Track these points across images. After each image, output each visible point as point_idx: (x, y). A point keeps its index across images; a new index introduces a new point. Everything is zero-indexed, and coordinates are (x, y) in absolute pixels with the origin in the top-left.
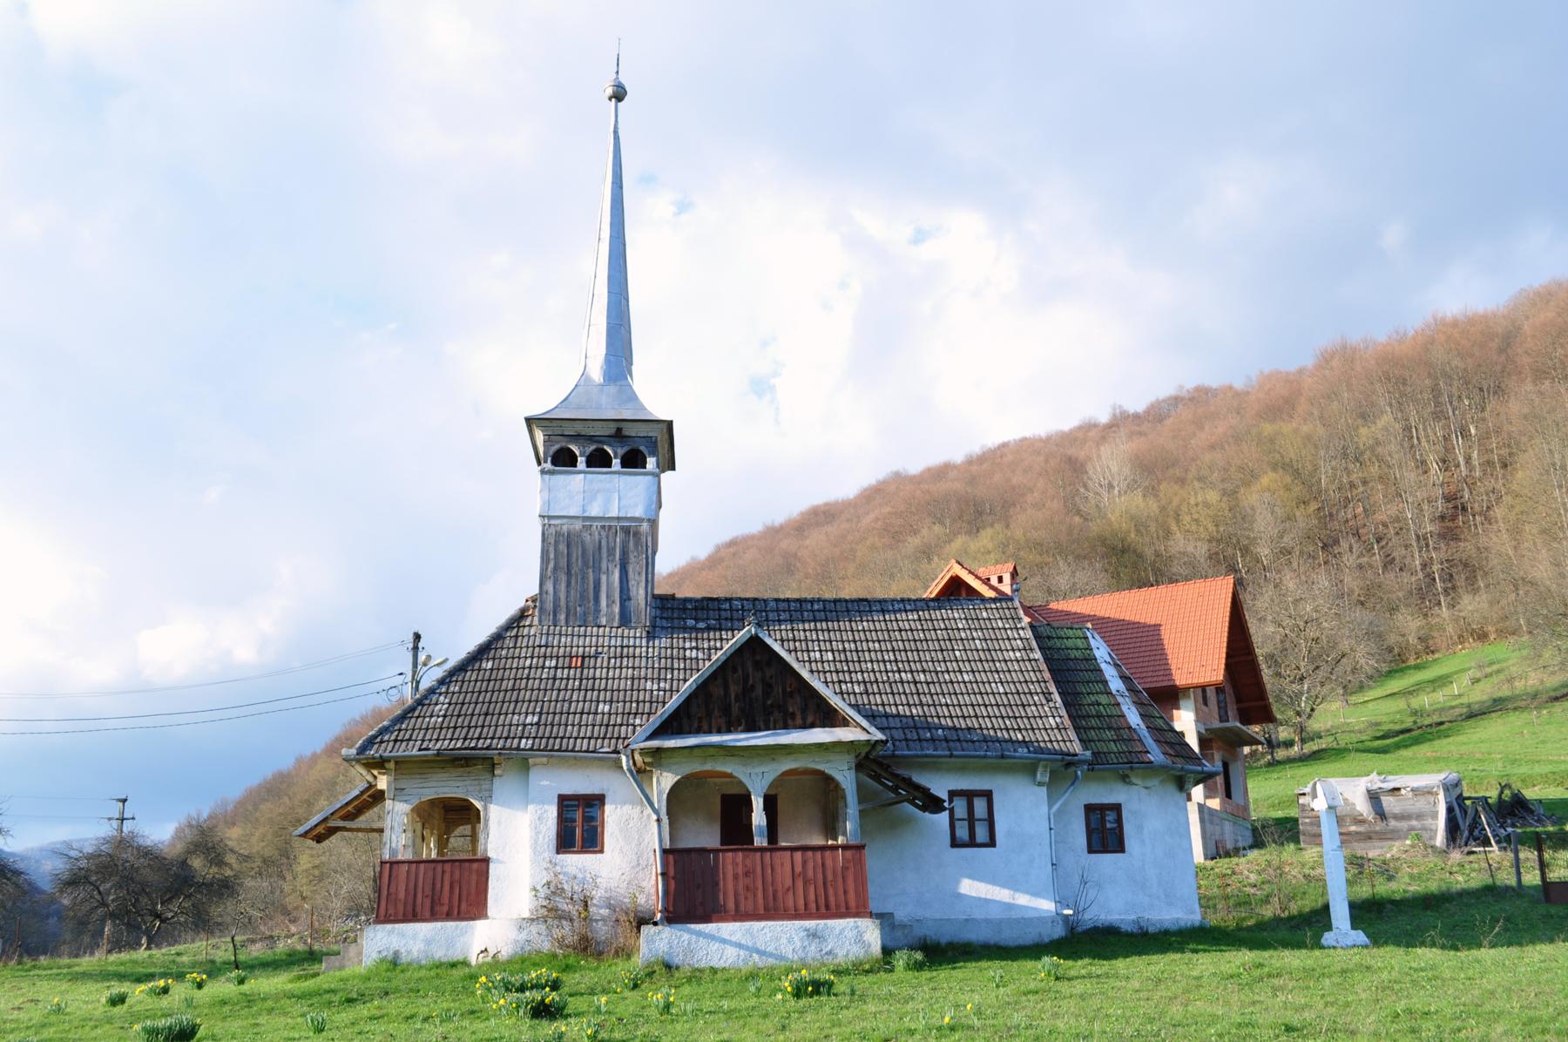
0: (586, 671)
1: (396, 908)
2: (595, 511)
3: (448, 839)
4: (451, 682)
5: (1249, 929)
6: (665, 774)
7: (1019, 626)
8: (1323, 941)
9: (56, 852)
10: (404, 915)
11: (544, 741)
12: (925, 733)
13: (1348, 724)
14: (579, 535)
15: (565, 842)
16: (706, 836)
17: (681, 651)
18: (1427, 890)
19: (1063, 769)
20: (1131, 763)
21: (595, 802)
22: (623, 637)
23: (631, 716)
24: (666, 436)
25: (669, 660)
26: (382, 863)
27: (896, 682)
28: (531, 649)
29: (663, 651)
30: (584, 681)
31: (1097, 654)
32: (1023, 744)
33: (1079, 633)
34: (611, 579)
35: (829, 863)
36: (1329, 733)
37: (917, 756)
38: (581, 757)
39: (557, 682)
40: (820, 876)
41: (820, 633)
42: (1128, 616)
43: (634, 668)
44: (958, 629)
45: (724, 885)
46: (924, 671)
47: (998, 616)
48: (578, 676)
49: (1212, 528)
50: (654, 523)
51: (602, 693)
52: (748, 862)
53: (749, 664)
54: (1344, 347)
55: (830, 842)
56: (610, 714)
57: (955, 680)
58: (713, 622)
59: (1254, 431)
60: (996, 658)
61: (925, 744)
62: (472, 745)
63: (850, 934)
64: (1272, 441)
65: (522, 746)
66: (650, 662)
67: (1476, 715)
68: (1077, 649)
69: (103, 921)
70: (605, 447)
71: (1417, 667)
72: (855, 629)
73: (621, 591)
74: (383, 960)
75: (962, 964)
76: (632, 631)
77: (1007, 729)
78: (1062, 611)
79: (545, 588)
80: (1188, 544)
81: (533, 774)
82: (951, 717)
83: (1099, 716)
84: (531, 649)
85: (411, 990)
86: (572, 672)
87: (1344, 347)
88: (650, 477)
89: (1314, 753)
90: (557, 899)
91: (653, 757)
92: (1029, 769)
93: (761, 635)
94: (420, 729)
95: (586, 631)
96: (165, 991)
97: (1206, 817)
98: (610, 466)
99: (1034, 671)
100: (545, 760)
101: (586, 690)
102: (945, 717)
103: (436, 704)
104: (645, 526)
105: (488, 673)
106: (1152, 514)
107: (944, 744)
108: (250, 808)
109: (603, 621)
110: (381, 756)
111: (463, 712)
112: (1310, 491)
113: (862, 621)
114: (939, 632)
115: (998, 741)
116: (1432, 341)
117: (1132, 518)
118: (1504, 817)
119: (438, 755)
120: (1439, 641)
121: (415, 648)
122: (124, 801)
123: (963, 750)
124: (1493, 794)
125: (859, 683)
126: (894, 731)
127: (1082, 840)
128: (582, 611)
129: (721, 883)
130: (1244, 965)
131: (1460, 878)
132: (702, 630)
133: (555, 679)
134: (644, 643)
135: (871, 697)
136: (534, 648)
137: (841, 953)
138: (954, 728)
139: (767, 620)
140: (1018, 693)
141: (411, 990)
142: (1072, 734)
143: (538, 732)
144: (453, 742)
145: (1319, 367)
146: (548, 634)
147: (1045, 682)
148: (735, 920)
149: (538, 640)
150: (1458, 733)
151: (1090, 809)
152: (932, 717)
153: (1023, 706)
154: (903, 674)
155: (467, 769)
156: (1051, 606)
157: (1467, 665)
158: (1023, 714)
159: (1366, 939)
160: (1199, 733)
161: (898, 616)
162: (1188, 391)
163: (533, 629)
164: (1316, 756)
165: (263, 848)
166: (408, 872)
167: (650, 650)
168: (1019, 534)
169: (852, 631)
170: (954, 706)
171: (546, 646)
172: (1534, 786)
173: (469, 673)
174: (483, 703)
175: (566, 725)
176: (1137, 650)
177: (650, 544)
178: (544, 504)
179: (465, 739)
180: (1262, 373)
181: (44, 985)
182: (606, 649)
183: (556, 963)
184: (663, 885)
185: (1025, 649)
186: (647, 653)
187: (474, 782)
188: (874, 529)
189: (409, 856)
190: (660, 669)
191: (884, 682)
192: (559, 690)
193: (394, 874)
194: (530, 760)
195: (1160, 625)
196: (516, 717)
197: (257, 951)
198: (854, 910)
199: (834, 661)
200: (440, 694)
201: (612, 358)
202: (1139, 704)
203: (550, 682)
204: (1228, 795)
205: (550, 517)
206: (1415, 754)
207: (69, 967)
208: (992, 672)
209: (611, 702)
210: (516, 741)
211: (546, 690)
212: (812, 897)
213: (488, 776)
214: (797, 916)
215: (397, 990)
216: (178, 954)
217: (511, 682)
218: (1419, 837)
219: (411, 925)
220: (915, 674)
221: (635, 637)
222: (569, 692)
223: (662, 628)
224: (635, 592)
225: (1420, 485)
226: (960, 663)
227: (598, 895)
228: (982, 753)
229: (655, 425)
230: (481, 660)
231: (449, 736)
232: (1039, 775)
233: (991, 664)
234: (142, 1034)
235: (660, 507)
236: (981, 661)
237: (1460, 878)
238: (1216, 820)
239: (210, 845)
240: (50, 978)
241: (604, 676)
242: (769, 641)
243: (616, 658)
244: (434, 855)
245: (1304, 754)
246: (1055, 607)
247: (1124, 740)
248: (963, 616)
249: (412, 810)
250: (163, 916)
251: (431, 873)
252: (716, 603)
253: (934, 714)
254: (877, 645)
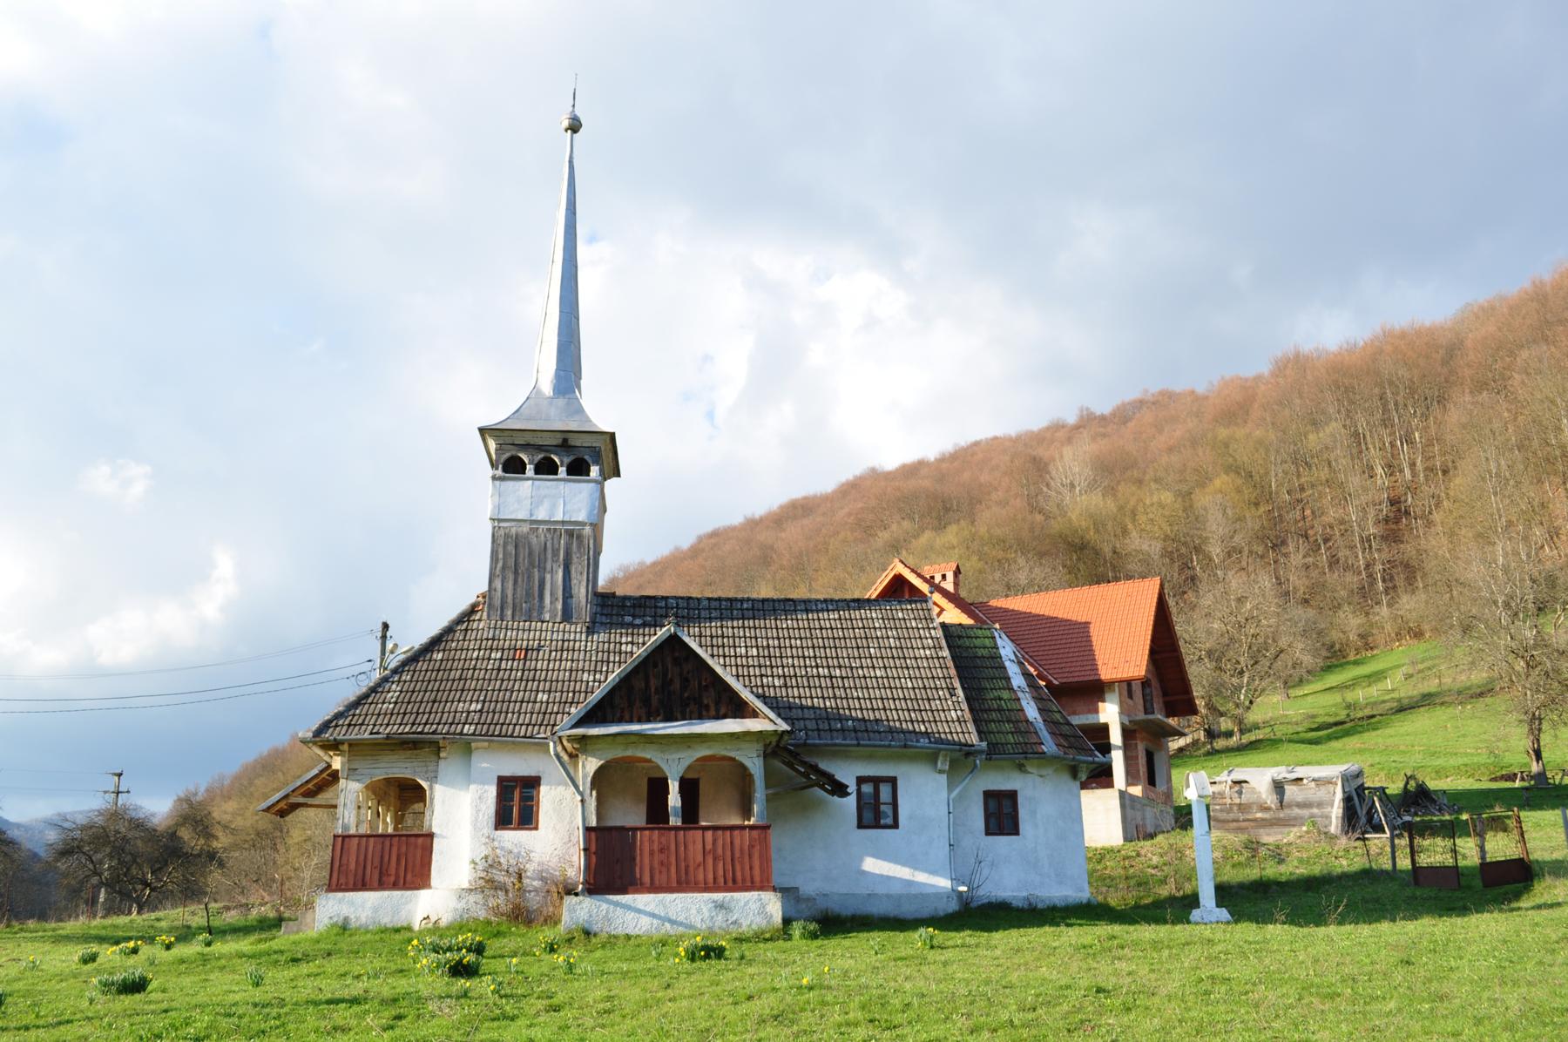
0: (528, 663)
1: (347, 878)
2: (541, 515)
3: (403, 815)
4: (403, 671)
5: (1147, 907)
6: (590, 759)
7: (931, 626)
8: (1191, 917)
9: (51, 824)
10: (355, 884)
11: (485, 727)
12: (836, 724)
13: (1286, 716)
14: (526, 537)
15: (503, 820)
16: (631, 815)
17: (618, 646)
18: (1311, 873)
19: (963, 758)
20: (1026, 753)
21: (531, 784)
22: (564, 632)
23: (567, 705)
24: (610, 446)
25: (606, 654)
26: (335, 836)
27: (813, 676)
28: (479, 642)
29: (601, 645)
30: (526, 672)
31: (1003, 652)
32: (925, 736)
33: (988, 633)
34: (555, 577)
35: (737, 842)
36: (1267, 724)
37: (826, 745)
38: (520, 742)
39: (502, 672)
40: (728, 853)
41: (747, 630)
42: (1061, 614)
43: (573, 661)
44: (875, 628)
45: (641, 861)
46: (840, 667)
47: (912, 616)
48: (521, 667)
49: (1168, 529)
50: (597, 527)
51: (542, 683)
52: (663, 840)
53: (669, 660)
54: (1297, 355)
55: (746, 823)
56: (548, 703)
57: (867, 675)
58: (649, 619)
59: (1210, 436)
60: (907, 656)
61: (835, 734)
62: (419, 730)
63: (754, 906)
64: (1227, 446)
65: (465, 731)
66: (588, 655)
67: (1405, 709)
68: (985, 648)
69: (97, 888)
70: (552, 456)
71: (1356, 663)
72: (779, 626)
73: (564, 590)
74: (334, 925)
75: (855, 934)
76: (573, 626)
77: (912, 721)
78: (1001, 608)
79: (493, 586)
80: (1143, 543)
81: (475, 757)
82: (861, 709)
83: (1000, 710)
84: (479, 642)
85: (351, 952)
86: (516, 663)
87: (1297, 355)
88: (592, 485)
89: (1251, 743)
90: (494, 871)
91: (579, 743)
92: (932, 758)
93: (679, 634)
94: (373, 715)
95: (530, 626)
96: (135, 951)
97: (1128, 802)
98: (556, 474)
99: (941, 668)
100: (486, 744)
101: (528, 681)
102: (856, 709)
103: (389, 692)
104: (587, 530)
105: (438, 664)
106: (1110, 513)
107: (853, 734)
108: (245, 783)
109: (547, 617)
110: (335, 739)
111: (413, 700)
112: (1262, 495)
113: (786, 619)
114: (857, 630)
115: (903, 731)
116: (1381, 351)
117: (1091, 516)
118: (1409, 806)
119: (387, 738)
120: (1380, 638)
121: (384, 637)
122: (120, 775)
123: (869, 740)
124: (1395, 788)
125: (779, 677)
126: (807, 722)
128: (529, 609)
129: (638, 858)
130: (1099, 937)
131: (1344, 863)
132: (638, 626)
133: (499, 670)
134: (584, 638)
135: (790, 690)
136: (482, 640)
137: (745, 923)
138: (863, 719)
139: (699, 618)
140: (925, 688)
141: (351, 952)
142: (971, 727)
143: (480, 718)
144: (402, 727)
145: (1274, 374)
146: (495, 628)
147: (951, 678)
148: (650, 892)
149: (485, 633)
150: (1387, 725)
151: (989, 795)
152: (844, 709)
153: (929, 700)
154: (820, 670)
155: (415, 752)
156: (990, 603)
157: (1403, 662)
158: (928, 707)
159: (1229, 916)
160: (1123, 725)
161: (820, 615)
162: (1153, 395)
163: (481, 623)
164: (1253, 746)
165: (257, 821)
166: (359, 844)
167: (589, 644)
168: (983, 530)
169: (777, 629)
170: (865, 699)
171: (493, 639)
172: (1447, 777)
173: (420, 664)
174: (432, 691)
175: (507, 713)
176: (1068, 646)
177: (591, 546)
178: (494, 507)
179: (413, 724)
180: (1223, 378)
181: (28, 947)
182: (548, 643)
183: (489, 928)
184: (585, 860)
185: (935, 648)
186: (586, 646)
187: (420, 764)
188: (846, 523)
189: (364, 829)
190: (597, 662)
191: (802, 677)
192: (503, 680)
193: (346, 846)
194: (473, 744)
195: (1090, 623)
196: (461, 705)
197: (232, 917)
198: (758, 884)
199: (758, 656)
200: (393, 682)
202: (1038, 699)
203: (495, 672)
204: (1152, 781)
205: (500, 520)
206: (1344, 745)
207: (54, 930)
208: (902, 668)
209: (550, 691)
210: (460, 726)
211: (490, 680)
212: (721, 872)
213: (434, 758)
214: (707, 889)
215: (340, 951)
216: (158, 920)
217: (459, 672)
218: (1314, 824)
219: (361, 893)
220: (832, 669)
221: (576, 632)
222: (511, 682)
223: (602, 623)
224: (576, 591)
225: (1365, 490)
226: (874, 660)
227: (531, 868)
228: (887, 743)
229: (599, 437)
230: (432, 652)
231: (399, 721)
233: (902, 661)
234: (99, 986)
235: (605, 511)
236: (893, 658)
237: (1344, 863)
238: (1138, 806)
239: (199, 818)
240: (33, 940)
241: (545, 667)
242: (686, 639)
243: (556, 651)
244: (390, 830)
245: (1242, 744)
246: (995, 605)
247: (1021, 732)
248: (880, 616)
249: (367, 787)
250: (153, 886)
251: (379, 847)
252: (653, 601)
253: (846, 706)
254: (798, 642)
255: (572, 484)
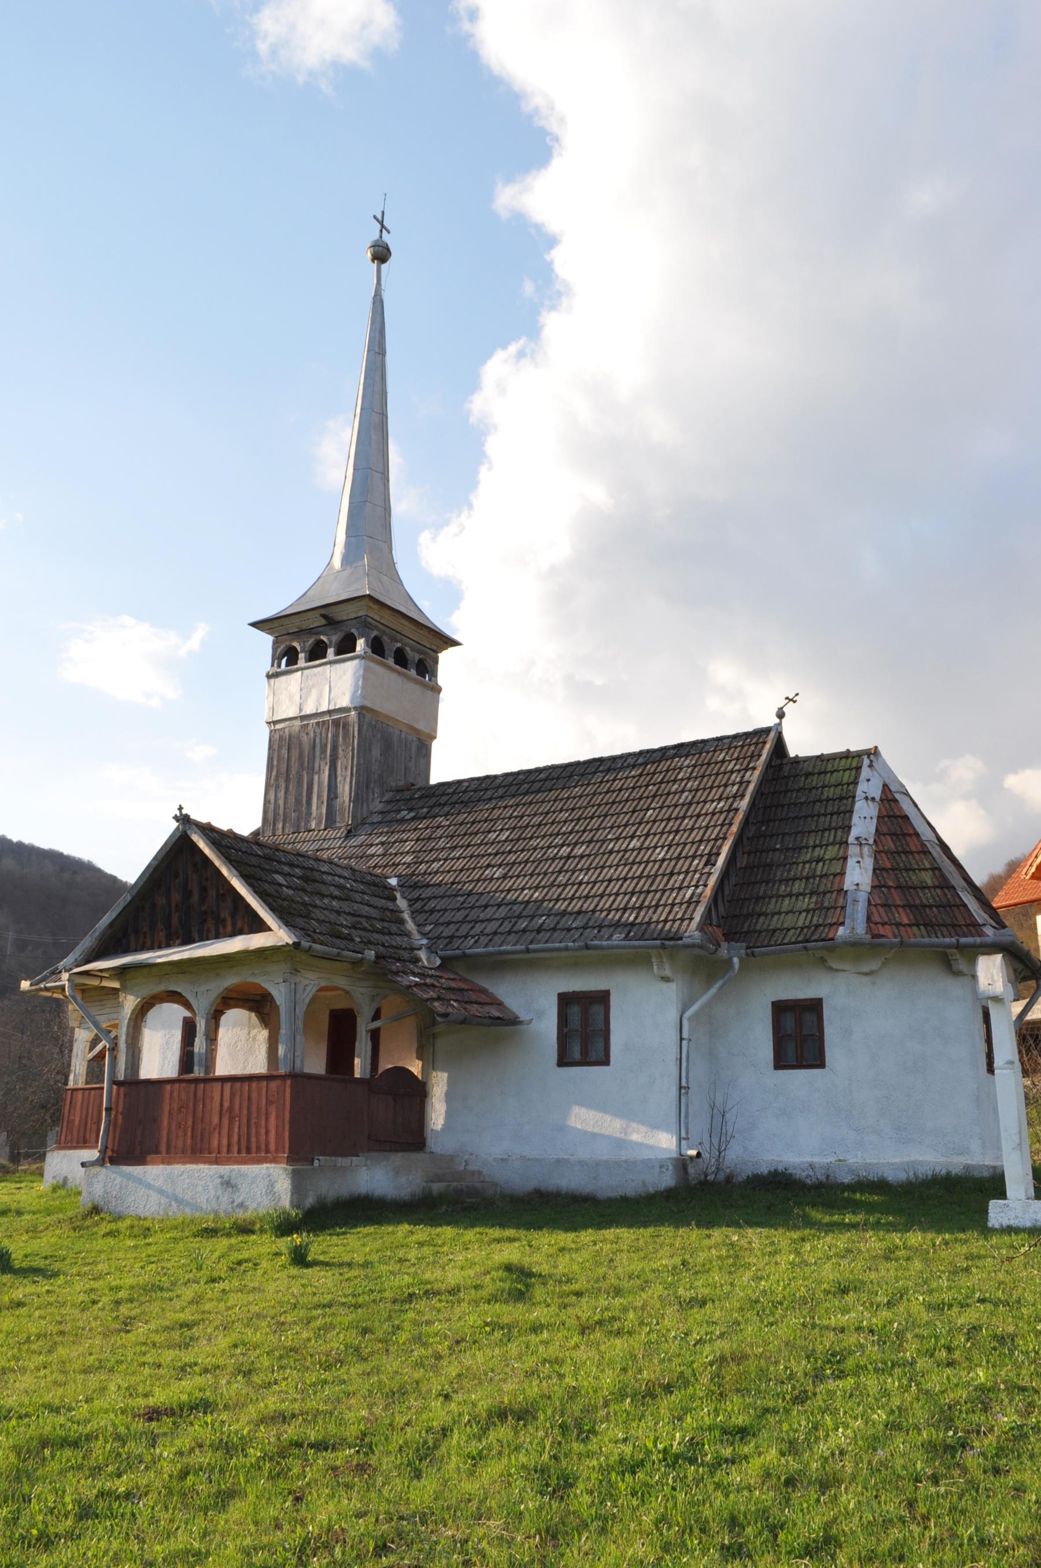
2: (309, 709)
40: (245, 1112)
88: (356, 662)
98: (325, 657)
127: (766, 1051)
151: (780, 1008)
166: (172, 1092)
201: (353, 540)
205: (275, 723)
232: (655, 967)
255: (338, 666)
